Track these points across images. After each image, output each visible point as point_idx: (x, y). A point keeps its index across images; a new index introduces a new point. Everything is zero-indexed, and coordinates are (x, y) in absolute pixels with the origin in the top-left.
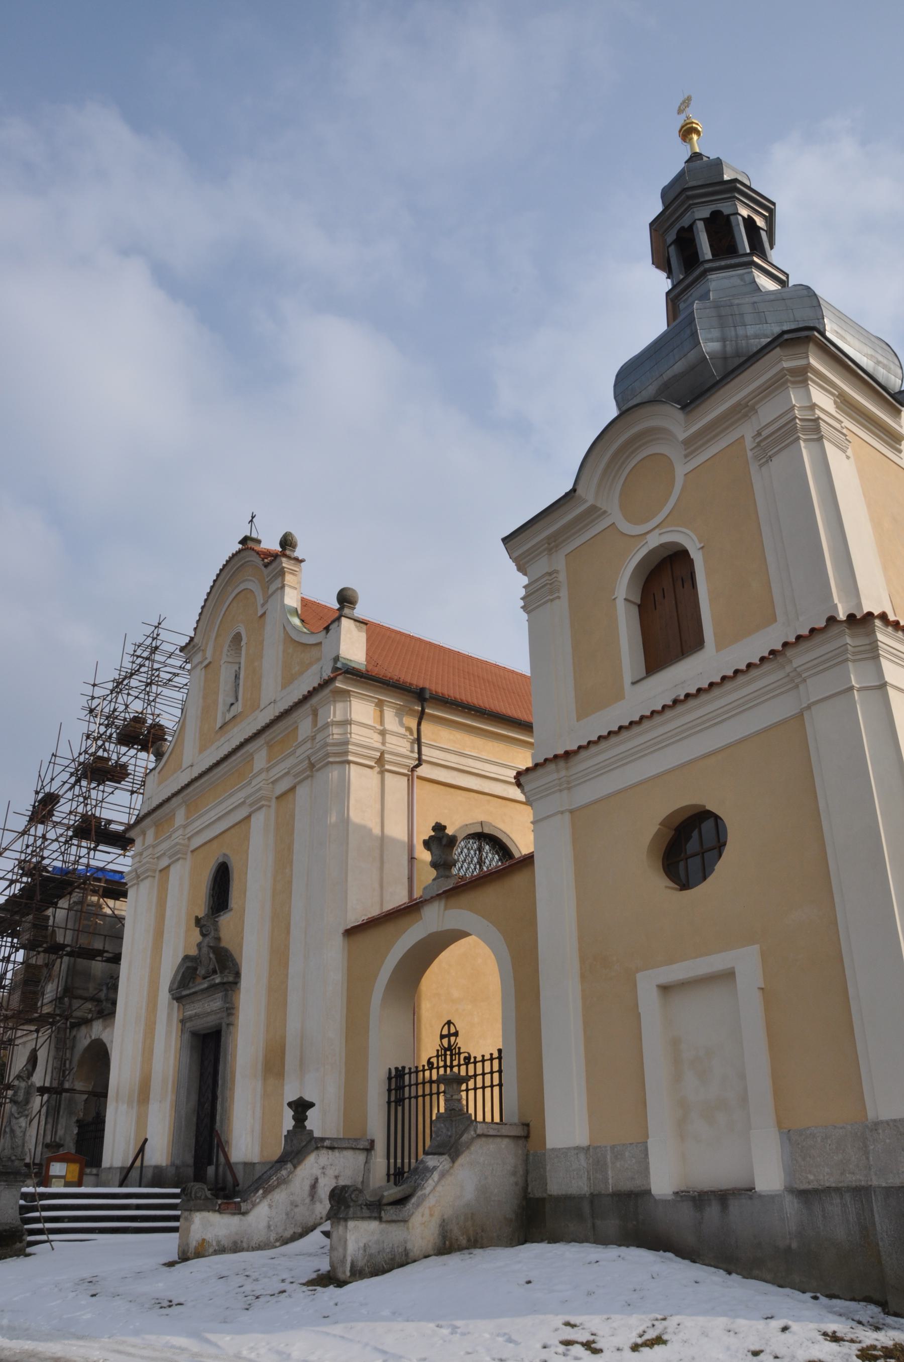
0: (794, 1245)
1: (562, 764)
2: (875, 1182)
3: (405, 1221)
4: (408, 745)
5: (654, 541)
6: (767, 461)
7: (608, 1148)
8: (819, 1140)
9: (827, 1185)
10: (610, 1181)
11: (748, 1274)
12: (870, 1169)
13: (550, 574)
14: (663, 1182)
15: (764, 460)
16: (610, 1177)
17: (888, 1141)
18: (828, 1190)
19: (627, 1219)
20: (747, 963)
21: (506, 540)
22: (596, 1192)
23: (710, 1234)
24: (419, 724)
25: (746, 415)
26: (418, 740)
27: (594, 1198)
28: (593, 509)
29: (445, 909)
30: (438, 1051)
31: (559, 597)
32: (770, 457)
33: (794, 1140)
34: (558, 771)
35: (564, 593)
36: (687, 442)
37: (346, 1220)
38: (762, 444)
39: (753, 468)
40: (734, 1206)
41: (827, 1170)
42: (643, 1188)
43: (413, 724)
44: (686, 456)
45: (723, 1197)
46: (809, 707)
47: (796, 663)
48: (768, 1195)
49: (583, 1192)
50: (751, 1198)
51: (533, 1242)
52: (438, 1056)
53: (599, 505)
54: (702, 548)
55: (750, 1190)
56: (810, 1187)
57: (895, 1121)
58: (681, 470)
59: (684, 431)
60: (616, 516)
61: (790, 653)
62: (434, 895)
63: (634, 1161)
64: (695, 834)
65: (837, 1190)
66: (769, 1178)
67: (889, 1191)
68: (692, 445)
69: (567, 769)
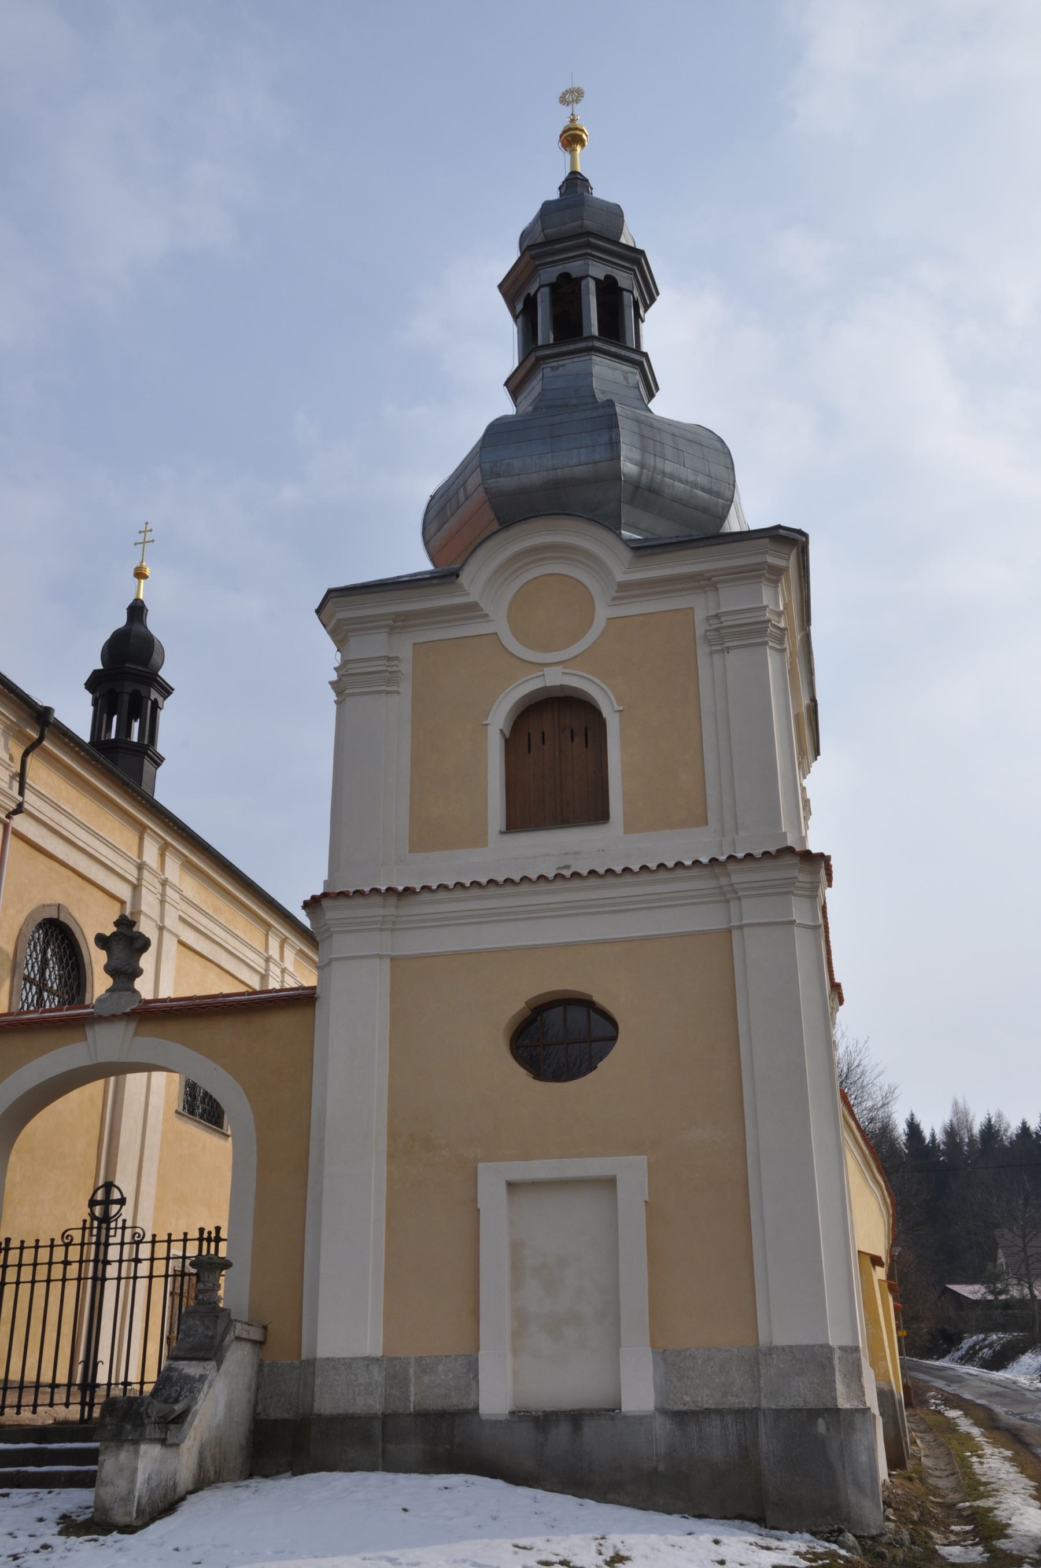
0: (661, 1467)
1: (392, 900)
2: (764, 1404)
3: (177, 1445)
4: (7, 779)
5: (554, 678)
6: (722, 651)
7: (413, 1360)
8: (700, 1362)
9: (705, 1406)
10: (412, 1398)
11: (602, 1497)
12: (760, 1392)
13: (389, 659)
14: (495, 1398)
15: (720, 648)
16: (412, 1394)
17: (782, 1366)
18: (706, 1412)
19: (442, 1441)
20: (633, 1173)
22: (389, 1411)
23: (560, 1455)
24: (26, 754)
25: (702, 587)
26: (22, 776)
27: (388, 1419)
28: (474, 606)
29: (135, 1034)
30: (85, 1221)
31: (398, 692)
32: (728, 648)
33: (670, 1361)
34: (384, 906)
35: (406, 688)
36: (623, 586)
37: (136, 1442)
38: (722, 631)
39: (702, 651)
40: (589, 1428)
41: (706, 1391)
42: (461, 1407)
43: (18, 752)
44: (614, 599)
45: (576, 1418)
46: (741, 927)
47: (735, 878)
48: (635, 1416)
49: (373, 1412)
50: (612, 1418)
51: (331, 1469)
52: (84, 1229)
53: (482, 605)
54: (620, 711)
55: (613, 1411)
56: (685, 1408)
57: (791, 1347)
58: (603, 612)
59: (625, 573)
60: (499, 624)
61: (731, 867)
62: (119, 1012)
63: (451, 1376)
65: (719, 1412)
66: (639, 1396)
67: (779, 1413)
68: (627, 591)
69: (397, 906)
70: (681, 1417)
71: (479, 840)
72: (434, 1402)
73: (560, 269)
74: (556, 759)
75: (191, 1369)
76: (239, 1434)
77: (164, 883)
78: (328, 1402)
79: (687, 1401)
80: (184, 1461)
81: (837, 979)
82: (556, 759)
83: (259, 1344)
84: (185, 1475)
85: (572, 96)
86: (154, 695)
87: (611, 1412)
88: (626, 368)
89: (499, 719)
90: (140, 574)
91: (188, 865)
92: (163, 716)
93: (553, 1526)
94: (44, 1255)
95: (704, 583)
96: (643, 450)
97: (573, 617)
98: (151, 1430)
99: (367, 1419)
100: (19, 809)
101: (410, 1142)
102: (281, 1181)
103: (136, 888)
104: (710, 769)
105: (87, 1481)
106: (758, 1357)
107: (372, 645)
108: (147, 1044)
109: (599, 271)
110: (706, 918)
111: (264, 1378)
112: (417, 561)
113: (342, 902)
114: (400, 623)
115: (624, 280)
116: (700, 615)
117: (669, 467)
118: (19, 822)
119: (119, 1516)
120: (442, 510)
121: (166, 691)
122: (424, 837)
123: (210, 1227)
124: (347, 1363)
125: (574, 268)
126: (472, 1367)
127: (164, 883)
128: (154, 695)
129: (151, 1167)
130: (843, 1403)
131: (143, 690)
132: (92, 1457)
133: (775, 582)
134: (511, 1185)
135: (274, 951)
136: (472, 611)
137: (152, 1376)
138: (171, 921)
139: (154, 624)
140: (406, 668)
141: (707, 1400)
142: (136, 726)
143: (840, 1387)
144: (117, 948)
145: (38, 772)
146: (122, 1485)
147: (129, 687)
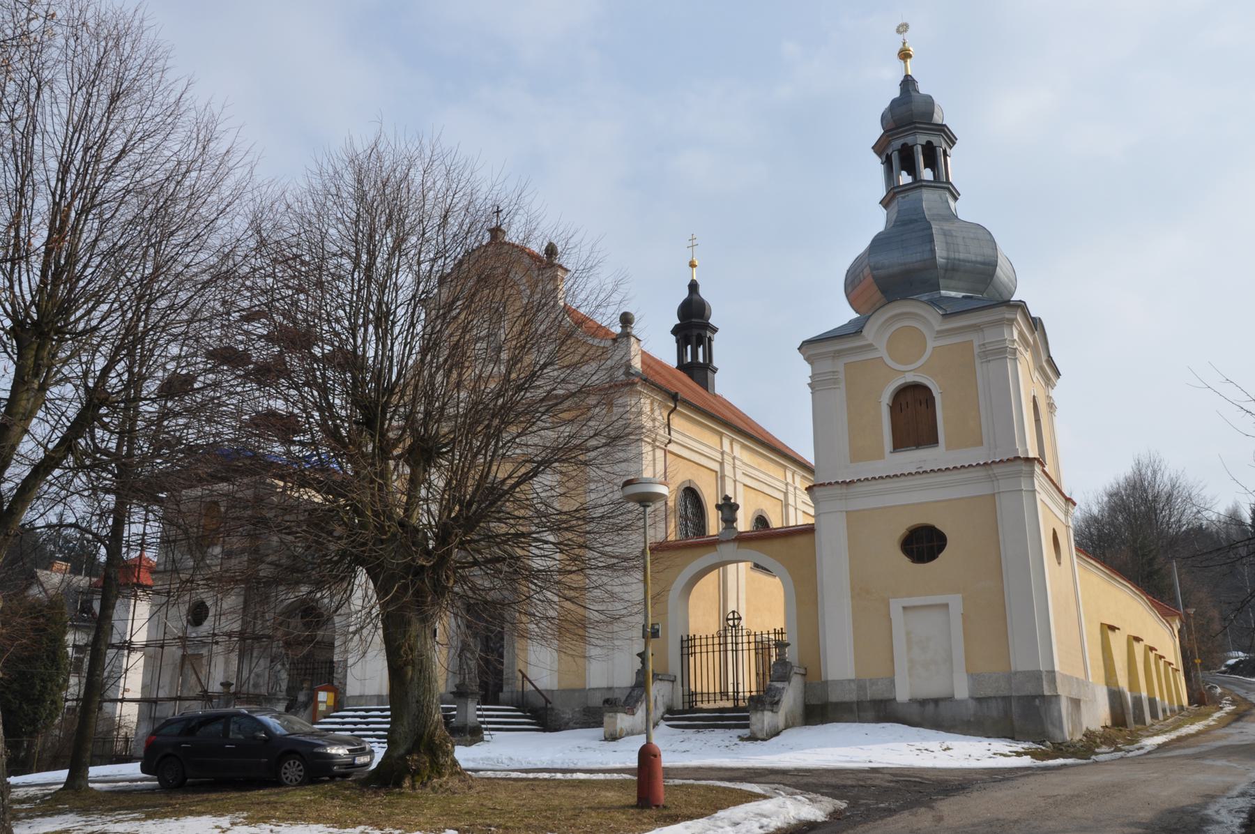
5: (910, 378)
18: (990, 698)
20: (956, 602)
21: (807, 347)
28: (871, 345)
33: (974, 678)
35: (842, 385)
36: (938, 332)
39: (978, 361)
40: (942, 705)
43: (665, 414)
45: (936, 701)
58: (931, 344)
60: (882, 352)
64: (15, 357)
66: (962, 691)
67: (1020, 698)
68: (941, 334)
70: (979, 700)
71: (881, 456)
72: (879, 697)
73: (902, 141)
74: (913, 416)
75: (779, 685)
76: (799, 710)
77: (734, 458)
78: (834, 697)
79: (982, 694)
80: (780, 718)
81: (1068, 495)
82: (913, 416)
83: (804, 675)
84: (781, 724)
85: (903, 28)
86: (709, 334)
87: (950, 699)
88: (941, 192)
89: (886, 398)
90: (692, 265)
91: (744, 446)
92: (714, 344)
93: (924, 739)
94: (710, 641)
95: (976, 328)
96: (948, 250)
97: (917, 346)
98: (767, 707)
99: (852, 703)
100: (670, 441)
101: (860, 592)
102: (805, 598)
103: (722, 464)
104: (983, 419)
105: (747, 726)
106: (1010, 676)
107: (826, 366)
108: (744, 551)
109: (922, 139)
110: (983, 489)
111: (807, 689)
112: (845, 314)
113: (822, 488)
114: (838, 354)
115: (935, 140)
116: (976, 344)
117: (962, 256)
118: (671, 447)
119: (760, 736)
120: (853, 281)
121: (715, 330)
122: (857, 455)
123: (778, 628)
124: (841, 682)
125: (909, 140)
126: (892, 682)
127: (734, 458)
128: (709, 334)
129: (742, 596)
130: (1047, 693)
131: (702, 332)
132: (747, 718)
133: (1011, 325)
134: (904, 608)
135: (790, 480)
136: (870, 347)
137: (754, 688)
138: (739, 477)
139: (704, 293)
140: (841, 376)
141: (990, 692)
142: (700, 350)
143: (1045, 686)
144: (726, 510)
145: (677, 422)
146: (759, 726)
147: (695, 332)
